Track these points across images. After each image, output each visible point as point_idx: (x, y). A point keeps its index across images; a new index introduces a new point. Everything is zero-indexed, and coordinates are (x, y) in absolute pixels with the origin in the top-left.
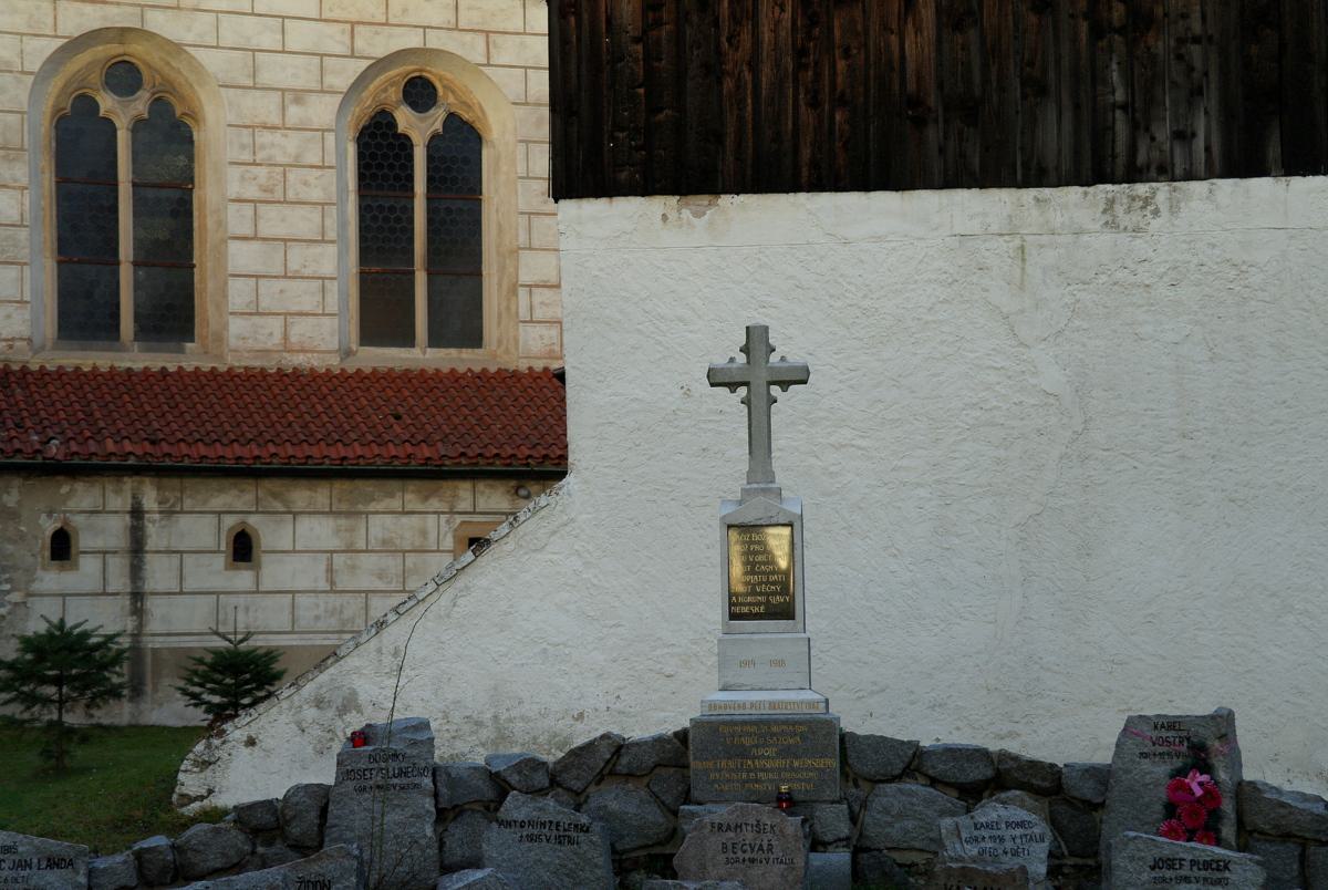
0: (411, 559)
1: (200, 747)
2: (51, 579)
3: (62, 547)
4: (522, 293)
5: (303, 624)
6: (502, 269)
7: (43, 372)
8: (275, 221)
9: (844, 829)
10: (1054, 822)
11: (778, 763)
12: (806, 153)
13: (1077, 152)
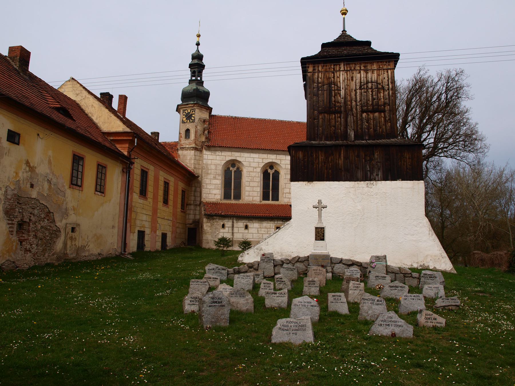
0: (269, 229)
1: (241, 254)
2: (222, 230)
3: (223, 226)
4: (284, 194)
5: (254, 238)
6: (282, 191)
7: (222, 203)
8: (252, 184)
9: (331, 270)
10: (360, 270)
11: (322, 261)
12: (325, 176)
13: (363, 176)
